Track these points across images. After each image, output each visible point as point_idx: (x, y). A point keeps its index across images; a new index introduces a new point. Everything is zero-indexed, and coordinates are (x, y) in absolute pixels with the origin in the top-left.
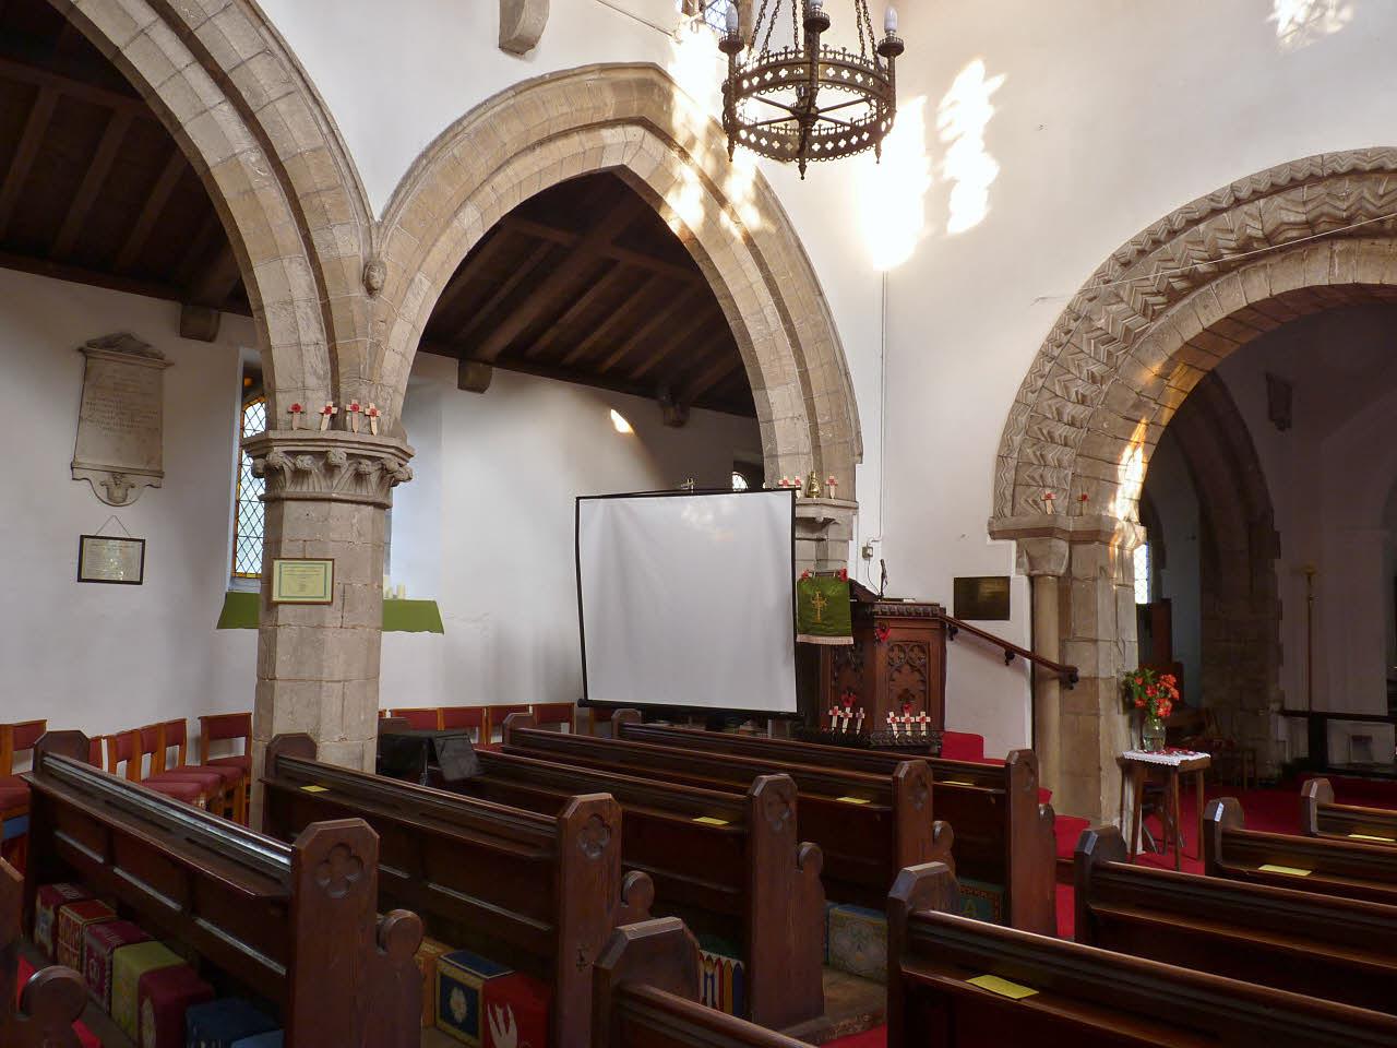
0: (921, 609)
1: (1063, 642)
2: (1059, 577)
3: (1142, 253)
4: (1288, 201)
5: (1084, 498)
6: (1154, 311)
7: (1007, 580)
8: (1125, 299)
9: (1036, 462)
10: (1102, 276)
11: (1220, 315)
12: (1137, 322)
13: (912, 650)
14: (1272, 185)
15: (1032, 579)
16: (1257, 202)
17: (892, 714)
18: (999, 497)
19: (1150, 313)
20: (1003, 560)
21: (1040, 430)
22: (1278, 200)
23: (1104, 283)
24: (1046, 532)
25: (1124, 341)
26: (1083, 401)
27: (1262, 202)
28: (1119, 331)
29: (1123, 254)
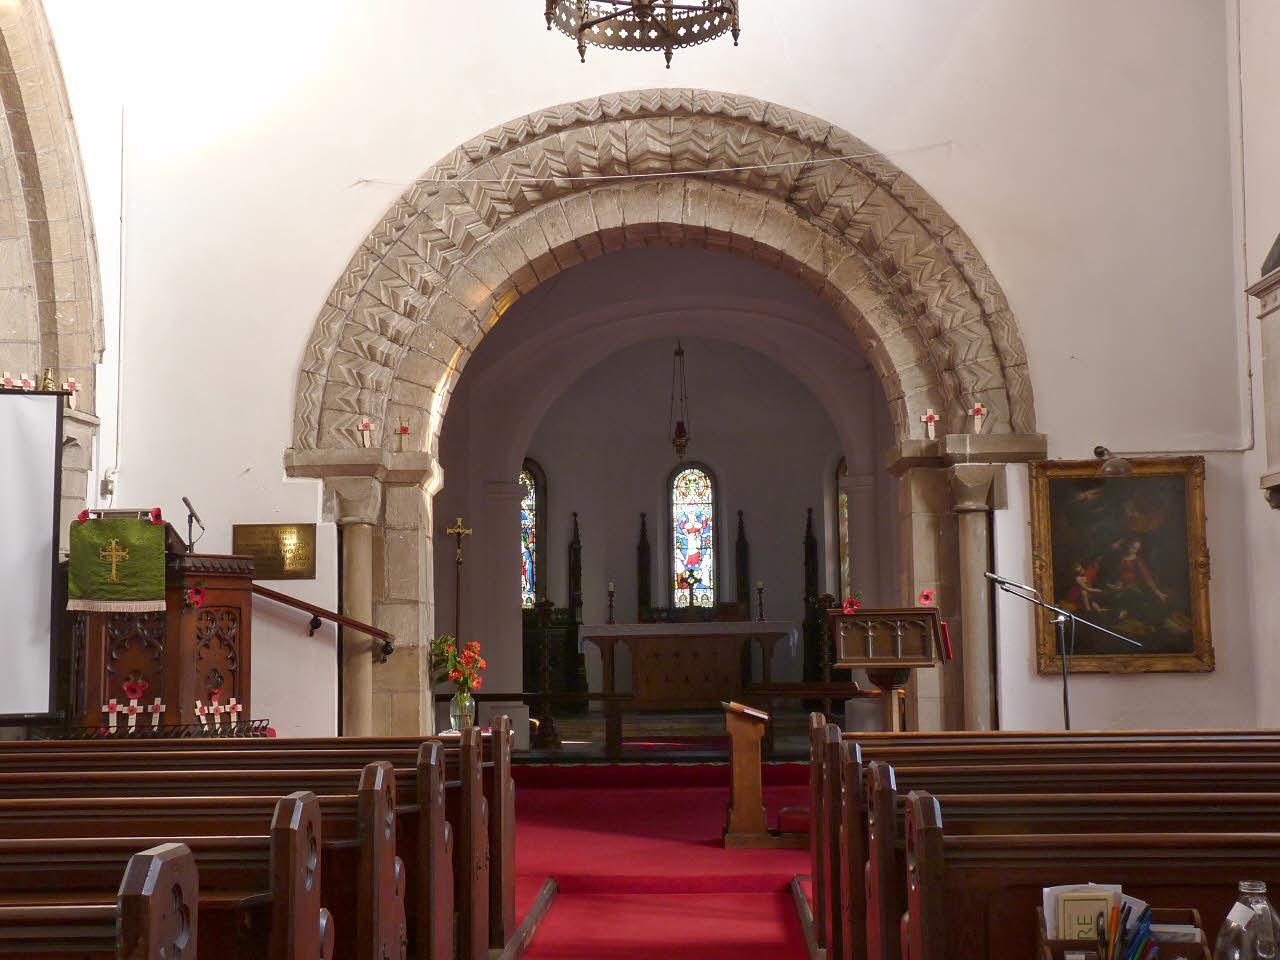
3: (495, 151)
4: (656, 128)
5: (404, 430)
6: (499, 219)
8: (471, 201)
10: (446, 168)
12: (479, 229)
14: (622, 110)
16: (623, 122)
17: (199, 703)
18: (301, 420)
19: (494, 220)
21: (359, 343)
23: (449, 178)
26: (410, 313)
27: (628, 124)
28: (460, 237)
29: (475, 149)
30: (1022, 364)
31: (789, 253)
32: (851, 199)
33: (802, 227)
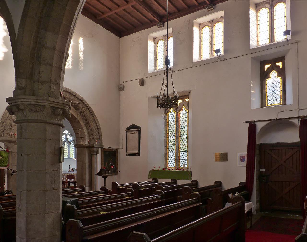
30: (101, 135)
31: (74, 115)
32: (84, 109)
33: (75, 111)
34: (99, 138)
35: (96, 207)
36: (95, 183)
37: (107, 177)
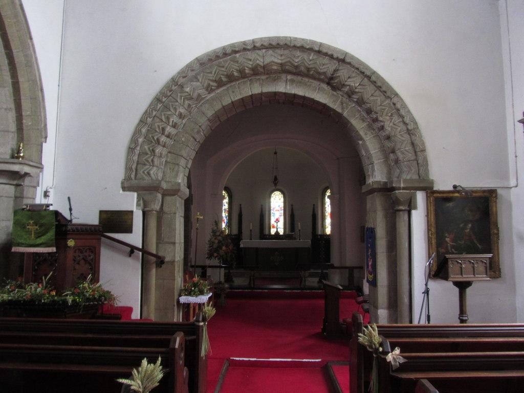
0: (88, 228)
1: (157, 244)
2: (157, 212)
6: (211, 89)
7: (132, 212)
8: (200, 80)
9: (149, 153)
11: (239, 97)
12: (202, 92)
13: (86, 252)
15: (144, 214)
18: (128, 169)
20: (129, 202)
22: (270, 52)
24: (153, 188)
25: (197, 100)
26: (174, 126)
27: (264, 50)
28: (195, 95)
30: (423, 151)
33: (333, 95)
34: (417, 160)
35: (47, 346)
36: (406, 300)
37: (469, 284)
